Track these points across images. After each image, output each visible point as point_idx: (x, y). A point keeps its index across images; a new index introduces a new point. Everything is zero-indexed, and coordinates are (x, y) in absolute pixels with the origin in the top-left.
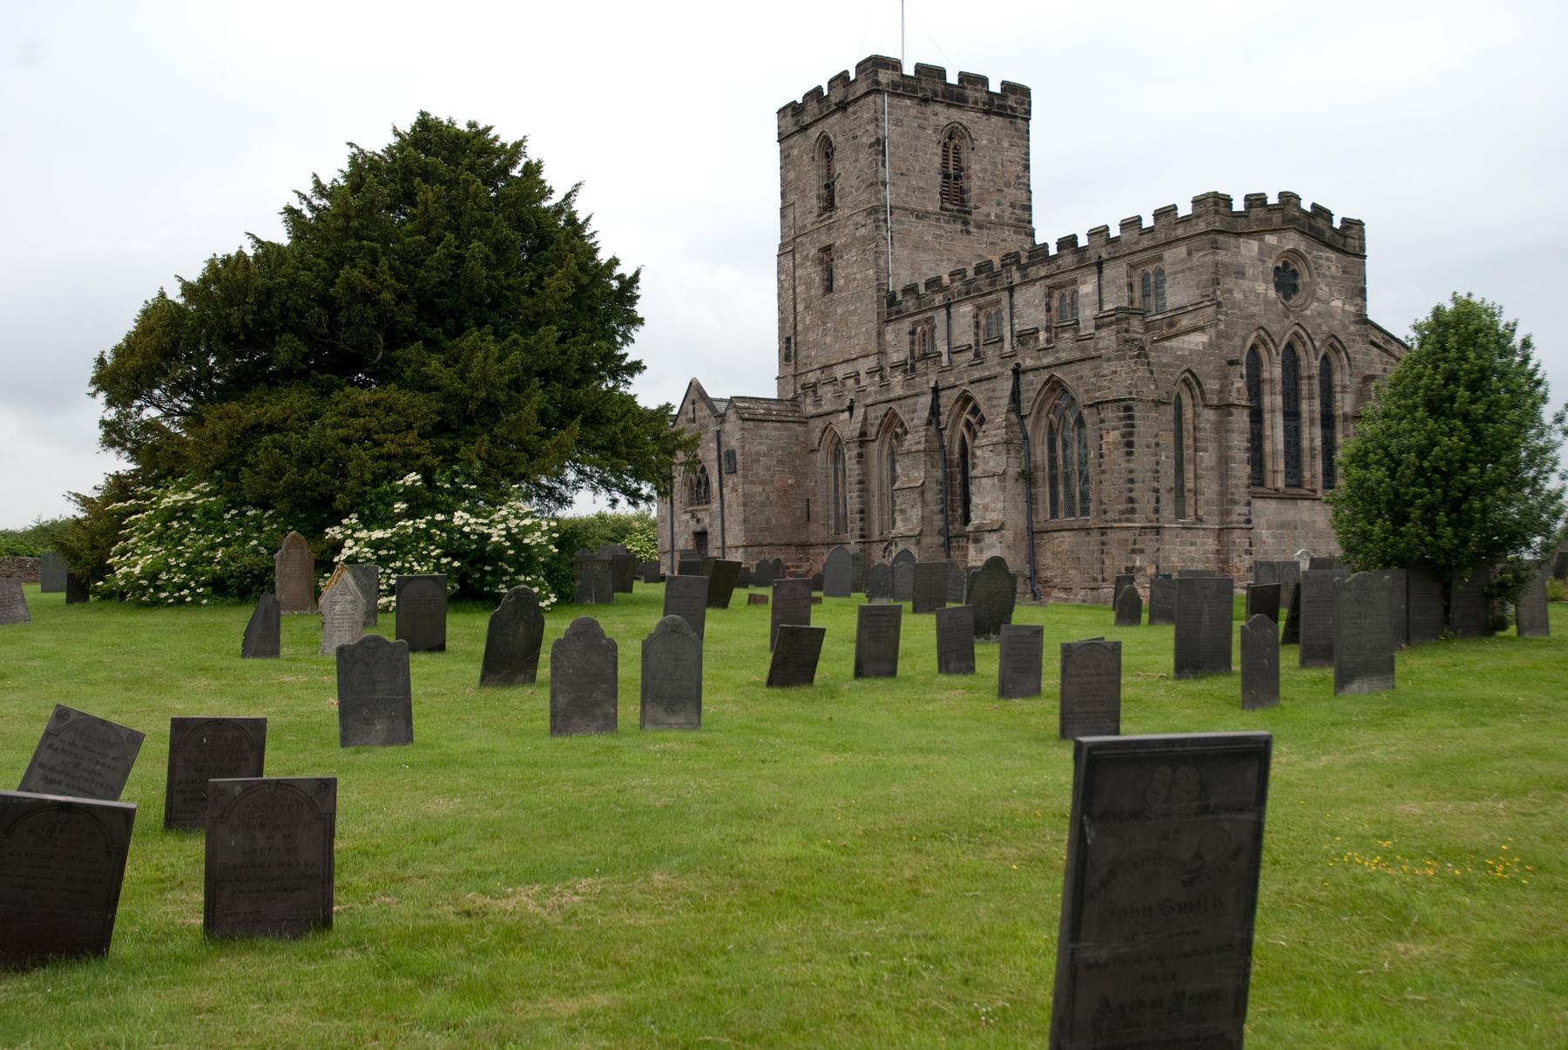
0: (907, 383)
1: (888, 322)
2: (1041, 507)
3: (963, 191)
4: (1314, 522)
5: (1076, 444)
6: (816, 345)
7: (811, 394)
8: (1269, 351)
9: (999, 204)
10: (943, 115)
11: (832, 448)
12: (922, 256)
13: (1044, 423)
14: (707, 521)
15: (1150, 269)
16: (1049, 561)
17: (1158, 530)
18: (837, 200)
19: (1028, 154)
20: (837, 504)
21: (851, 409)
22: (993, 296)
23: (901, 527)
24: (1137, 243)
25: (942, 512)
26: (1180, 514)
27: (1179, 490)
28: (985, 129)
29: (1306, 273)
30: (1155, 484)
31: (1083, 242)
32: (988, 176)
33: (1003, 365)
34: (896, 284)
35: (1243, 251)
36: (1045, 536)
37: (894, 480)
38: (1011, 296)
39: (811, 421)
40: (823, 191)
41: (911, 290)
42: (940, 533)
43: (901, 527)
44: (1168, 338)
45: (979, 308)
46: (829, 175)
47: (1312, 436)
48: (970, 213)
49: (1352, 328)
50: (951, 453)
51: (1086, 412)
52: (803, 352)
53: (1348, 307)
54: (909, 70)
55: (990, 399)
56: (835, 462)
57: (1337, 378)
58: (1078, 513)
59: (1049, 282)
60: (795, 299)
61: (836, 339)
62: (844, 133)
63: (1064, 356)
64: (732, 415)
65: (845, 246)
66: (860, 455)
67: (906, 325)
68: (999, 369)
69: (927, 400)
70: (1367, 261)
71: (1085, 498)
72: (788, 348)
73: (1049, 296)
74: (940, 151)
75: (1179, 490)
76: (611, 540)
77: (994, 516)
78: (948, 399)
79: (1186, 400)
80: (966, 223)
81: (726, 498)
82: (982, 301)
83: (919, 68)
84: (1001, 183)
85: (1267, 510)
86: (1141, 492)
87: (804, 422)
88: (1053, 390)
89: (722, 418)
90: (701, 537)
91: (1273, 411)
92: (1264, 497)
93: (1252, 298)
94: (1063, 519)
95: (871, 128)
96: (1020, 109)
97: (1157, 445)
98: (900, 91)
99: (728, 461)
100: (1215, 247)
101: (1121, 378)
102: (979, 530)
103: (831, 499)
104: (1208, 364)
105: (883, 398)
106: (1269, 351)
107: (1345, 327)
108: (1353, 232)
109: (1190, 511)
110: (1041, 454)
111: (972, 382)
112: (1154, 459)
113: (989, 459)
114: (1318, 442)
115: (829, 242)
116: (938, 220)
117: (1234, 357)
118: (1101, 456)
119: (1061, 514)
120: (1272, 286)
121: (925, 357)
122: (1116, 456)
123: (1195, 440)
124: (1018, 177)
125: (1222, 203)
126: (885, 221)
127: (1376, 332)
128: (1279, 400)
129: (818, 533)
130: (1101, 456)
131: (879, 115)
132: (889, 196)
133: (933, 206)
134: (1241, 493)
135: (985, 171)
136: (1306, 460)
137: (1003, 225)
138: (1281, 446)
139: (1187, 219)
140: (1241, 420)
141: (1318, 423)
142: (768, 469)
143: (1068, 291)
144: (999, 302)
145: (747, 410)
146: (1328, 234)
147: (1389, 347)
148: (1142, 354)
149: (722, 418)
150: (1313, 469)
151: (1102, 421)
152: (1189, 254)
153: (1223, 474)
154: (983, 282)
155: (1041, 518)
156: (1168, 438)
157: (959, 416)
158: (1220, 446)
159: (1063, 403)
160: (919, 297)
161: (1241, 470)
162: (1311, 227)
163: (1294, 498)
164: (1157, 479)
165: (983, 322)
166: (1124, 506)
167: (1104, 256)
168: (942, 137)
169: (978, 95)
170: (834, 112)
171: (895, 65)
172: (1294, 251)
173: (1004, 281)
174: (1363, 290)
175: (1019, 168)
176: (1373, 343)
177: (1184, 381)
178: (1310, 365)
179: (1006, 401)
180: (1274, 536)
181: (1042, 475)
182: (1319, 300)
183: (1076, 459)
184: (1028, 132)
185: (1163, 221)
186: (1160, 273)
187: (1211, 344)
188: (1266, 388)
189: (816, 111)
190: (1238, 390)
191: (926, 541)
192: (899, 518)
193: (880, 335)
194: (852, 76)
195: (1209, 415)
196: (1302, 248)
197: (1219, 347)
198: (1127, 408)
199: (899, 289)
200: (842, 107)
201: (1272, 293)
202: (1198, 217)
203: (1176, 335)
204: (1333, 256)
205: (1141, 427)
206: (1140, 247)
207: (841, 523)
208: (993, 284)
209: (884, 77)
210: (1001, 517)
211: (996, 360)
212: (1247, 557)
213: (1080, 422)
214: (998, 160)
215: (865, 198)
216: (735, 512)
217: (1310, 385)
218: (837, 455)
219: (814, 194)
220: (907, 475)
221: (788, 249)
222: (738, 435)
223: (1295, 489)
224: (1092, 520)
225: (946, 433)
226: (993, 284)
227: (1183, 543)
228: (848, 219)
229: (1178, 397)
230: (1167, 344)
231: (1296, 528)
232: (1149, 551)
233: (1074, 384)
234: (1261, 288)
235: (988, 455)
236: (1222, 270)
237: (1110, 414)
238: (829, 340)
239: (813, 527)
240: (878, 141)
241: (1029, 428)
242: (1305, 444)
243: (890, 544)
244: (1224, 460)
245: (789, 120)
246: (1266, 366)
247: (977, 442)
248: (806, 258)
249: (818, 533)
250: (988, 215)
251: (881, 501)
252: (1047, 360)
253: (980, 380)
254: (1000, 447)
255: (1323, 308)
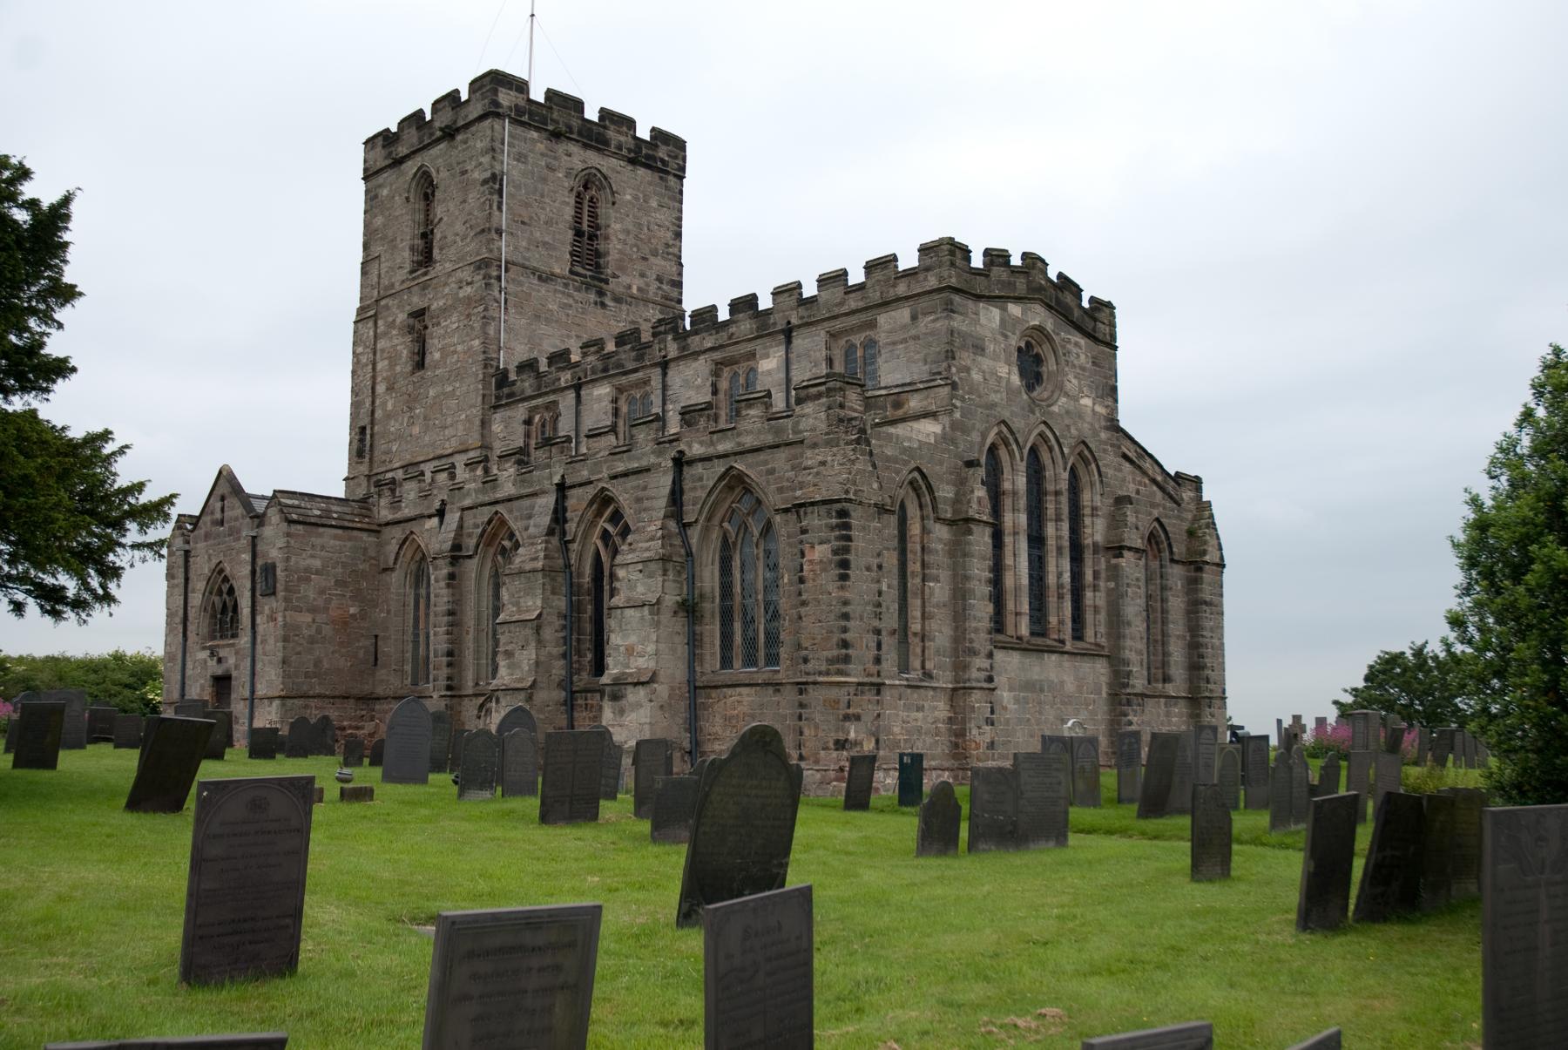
0: (521, 478)
1: (496, 407)
2: (707, 652)
3: (598, 254)
4: (1062, 683)
5: (761, 565)
6: (399, 437)
7: (387, 493)
8: (1011, 454)
9: (642, 275)
10: (578, 157)
11: (413, 567)
12: (543, 328)
13: (715, 535)
14: (232, 661)
15: (857, 339)
16: (718, 729)
17: (878, 688)
18: (436, 252)
19: (680, 219)
20: (416, 643)
21: (441, 513)
22: (640, 375)
23: (505, 676)
24: (841, 304)
25: (564, 656)
26: (904, 667)
27: (903, 632)
28: (630, 182)
29: (1052, 360)
30: (876, 623)
31: (765, 303)
32: (631, 240)
33: (659, 454)
34: (508, 360)
35: (983, 320)
36: (714, 693)
37: (497, 611)
38: (665, 374)
39: (387, 531)
40: (418, 242)
41: (528, 366)
42: (560, 685)
43: (505, 676)
44: (893, 422)
45: (620, 390)
46: (428, 221)
47: (1058, 569)
48: (607, 282)
49: (1104, 435)
50: (580, 575)
51: (778, 518)
52: (381, 446)
53: (1098, 409)
54: (538, 95)
55: (639, 500)
56: (417, 585)
57: (1086, 498)
58: (762, 662)
59: (717, 355)
60: (374, 378)
61: (426, 429)
62: (450, 168)
63: (749, 441)
64: (274, 517)
65: (444, 310)
66: (452, 576)
67: (521, 411)
68: (653, 459)
69: (549, 501)
70: (1120, 354)
71: (773, 639)
72: (362, 441)
73: (716, 374)
74: (572, 200)
75: (903, 632)
76: (127, 686)
77: (642, 664)
78: (578, 500)
79: (913, 510)
80: (601, 293)
81: (260, 629)
82: (624, 380)
83: (551, 94)
84: (646, 250)
85: (1010, 664)
86: (857, 632)
87: (376, 530)
88: (730, 488)
89: (259, 519)
90: (222, 683)
91: (1015, 533)
92: (1005, 648)
93: (992, 382)
94: (739, 670)
95: (485, 160)
96: (673, 165)
97: (880, 567)
98: (525, 118)
99: (264, 578)
100: (950, 309)
101: (831, 470)
102: (620, 683)
103: (409, 637)
104: (941, 463)
105: (487, 499)
106: (1011, 454)
107: (1095, 434)
108: (1102, 316)
109: (917, 663)
110: (709, 578)
111: (614, 477)
112: (875, 586)
113: (636, 581)
114: (1067, 577)
115: (422, 305)
116: (566, 285)
117: (974, 456)
118: (802, 581)
119: (737, 663)
120: (1015, 370)
121: (547, 443)
122: (828, 580)
123: (924, 565)
124: (667, 246)
125: (959, 254)
126: (499, 278)
127: (1128, 443)
128: (1023, 519)
129: (388, 680)
130: (802, 581)
131: (497, 145)
132: (504, 247)
133: (561, 267)
134: (981, 641)
135: (628, 232)
136: (1052, 600)
137: (646, 301)
138: (1025, 581)
139: (910, 273)
140: (981, 540)
141: (1067, 552)
142: (322, 592)
143: (741, 369)
144: (646, 382)
145: (296, 510)
146: (1077, 313)
147: (1141, 463)
148: (862, 439)
149: (259, 519)
150: (1060, 613)
151: (804, 531)
152: (914, 318)
153: (959, 615)
154: (627, 357)
155: (708, 668)
156: (891, 560)
157: (593, 524)
158: (955, 576)
159: (744, 507)
160: (539, 376)
161: (982, 610)
162: (1058, 301)
163: (1040, 650)
164: (878, 616)
165: (624, 409)
166: (835, 652)
167: (794, 321)
168: (576, 184)
169: (622, 139)
170: (438, 141)
171: (521, 86)
172: (1040, 329)
173: (656, 354)
174: (1114, 389)
175: (670, 235)
176: (1125, 457)
177: (911, 483)
178: (1057, 477)
179: (662, 503)
180: (1017, 701)
181: (711, 607)
182: (1067, 395)
183: (760, 586)
184: (681, 192)
185: (878, 275)
186: (870, 344)
187: (944, 436)
188: (1007, 502)
189: (415, 140)
190: (979, 500)
191: (541, 696)
192: (502, 663)
193: (484, 424)
194: (464, 96)
195: (941, 532)
196: (1049, 326)
197: (953, 441)
198: (840, 511)
199: (512, 368)
200: (449, 133)
201: (1016, 379)
202: (927, 269)
203: (903, 420)
204: (1083, 341)
205: (860, 542)
206: (845, 309)
207: (421, 670)
208: (640, 358)
209: (506, 98)
210: (652, 664)
211: (650, 446)
212: (988, 728)
213: (768, 529)
214: (644, 221)
215: (474, 249)
216: (271, 646)
217: (1057, 502)
218: (420, 577)
219: (406, 244)
220: (517, 604)
221: (368, 314)
222: (281, 543)
223: (1039, 642)
224: (783, 672)
225: (575, 546)
226: (640, 358)
227: (907, 708)
228: (449, 275)
229: (903, 506)
230: (891, 430)
231: (1042, 690)
232: (867, 718)
233: (762, 480)
234: (1003, 370)
235: (635, 576)
236: (958, 342)
237: (816, 521)
238: (416, 430)
239: (381, 673)
240: (494, 177)
241: (694, 541)
242: (1051, 579)
243: (489, 699)
244: (960, 594)
245: (379, 151)
246: (1007, 474)
247: (619, 559)
248: (392, 325)
249: (388, 680)
250: (629, 287)
251: (477, 640)
252: (724, 447)
253: (625, 474)
254: (653, 566)
255: (1071, 406)
